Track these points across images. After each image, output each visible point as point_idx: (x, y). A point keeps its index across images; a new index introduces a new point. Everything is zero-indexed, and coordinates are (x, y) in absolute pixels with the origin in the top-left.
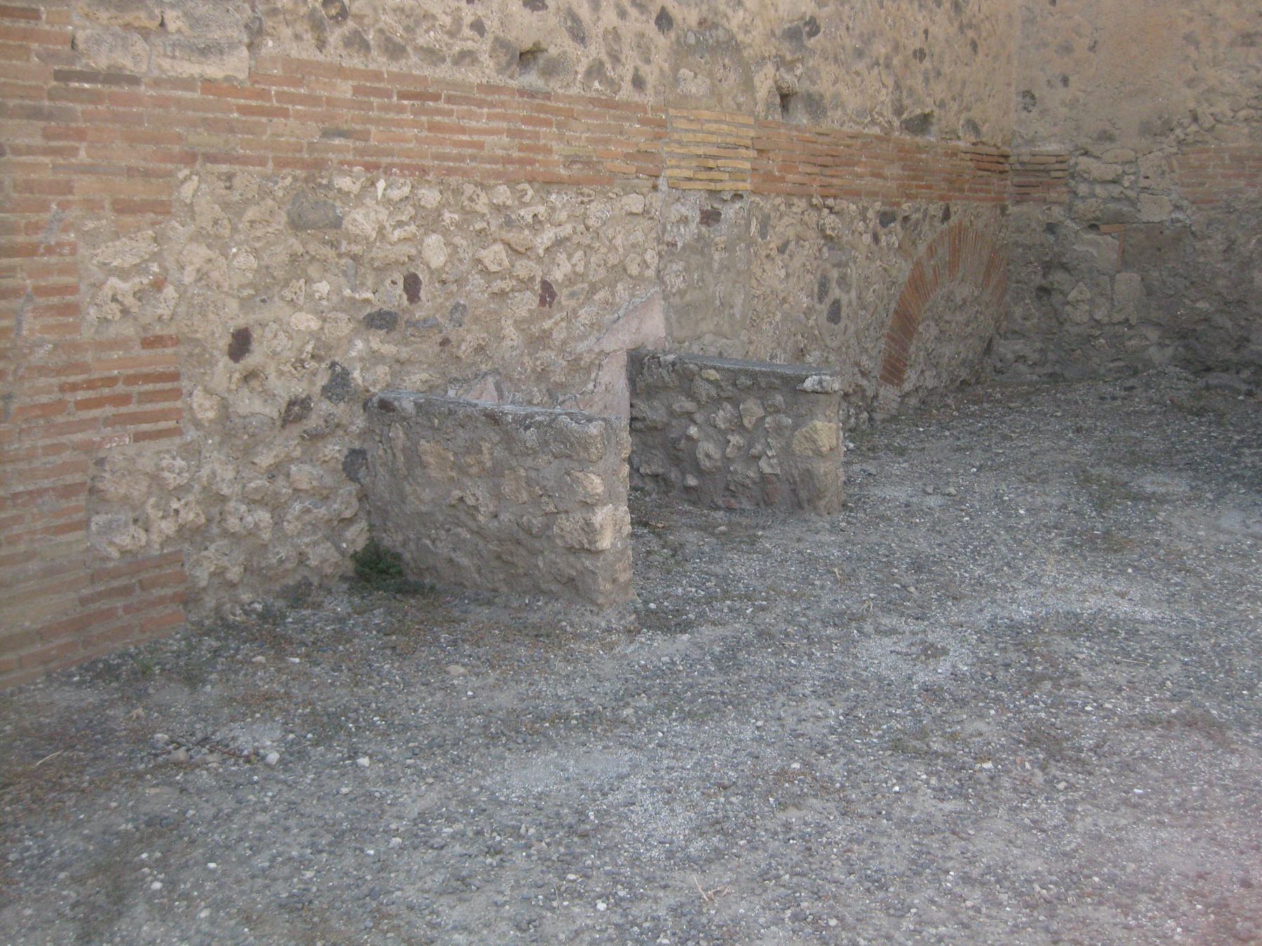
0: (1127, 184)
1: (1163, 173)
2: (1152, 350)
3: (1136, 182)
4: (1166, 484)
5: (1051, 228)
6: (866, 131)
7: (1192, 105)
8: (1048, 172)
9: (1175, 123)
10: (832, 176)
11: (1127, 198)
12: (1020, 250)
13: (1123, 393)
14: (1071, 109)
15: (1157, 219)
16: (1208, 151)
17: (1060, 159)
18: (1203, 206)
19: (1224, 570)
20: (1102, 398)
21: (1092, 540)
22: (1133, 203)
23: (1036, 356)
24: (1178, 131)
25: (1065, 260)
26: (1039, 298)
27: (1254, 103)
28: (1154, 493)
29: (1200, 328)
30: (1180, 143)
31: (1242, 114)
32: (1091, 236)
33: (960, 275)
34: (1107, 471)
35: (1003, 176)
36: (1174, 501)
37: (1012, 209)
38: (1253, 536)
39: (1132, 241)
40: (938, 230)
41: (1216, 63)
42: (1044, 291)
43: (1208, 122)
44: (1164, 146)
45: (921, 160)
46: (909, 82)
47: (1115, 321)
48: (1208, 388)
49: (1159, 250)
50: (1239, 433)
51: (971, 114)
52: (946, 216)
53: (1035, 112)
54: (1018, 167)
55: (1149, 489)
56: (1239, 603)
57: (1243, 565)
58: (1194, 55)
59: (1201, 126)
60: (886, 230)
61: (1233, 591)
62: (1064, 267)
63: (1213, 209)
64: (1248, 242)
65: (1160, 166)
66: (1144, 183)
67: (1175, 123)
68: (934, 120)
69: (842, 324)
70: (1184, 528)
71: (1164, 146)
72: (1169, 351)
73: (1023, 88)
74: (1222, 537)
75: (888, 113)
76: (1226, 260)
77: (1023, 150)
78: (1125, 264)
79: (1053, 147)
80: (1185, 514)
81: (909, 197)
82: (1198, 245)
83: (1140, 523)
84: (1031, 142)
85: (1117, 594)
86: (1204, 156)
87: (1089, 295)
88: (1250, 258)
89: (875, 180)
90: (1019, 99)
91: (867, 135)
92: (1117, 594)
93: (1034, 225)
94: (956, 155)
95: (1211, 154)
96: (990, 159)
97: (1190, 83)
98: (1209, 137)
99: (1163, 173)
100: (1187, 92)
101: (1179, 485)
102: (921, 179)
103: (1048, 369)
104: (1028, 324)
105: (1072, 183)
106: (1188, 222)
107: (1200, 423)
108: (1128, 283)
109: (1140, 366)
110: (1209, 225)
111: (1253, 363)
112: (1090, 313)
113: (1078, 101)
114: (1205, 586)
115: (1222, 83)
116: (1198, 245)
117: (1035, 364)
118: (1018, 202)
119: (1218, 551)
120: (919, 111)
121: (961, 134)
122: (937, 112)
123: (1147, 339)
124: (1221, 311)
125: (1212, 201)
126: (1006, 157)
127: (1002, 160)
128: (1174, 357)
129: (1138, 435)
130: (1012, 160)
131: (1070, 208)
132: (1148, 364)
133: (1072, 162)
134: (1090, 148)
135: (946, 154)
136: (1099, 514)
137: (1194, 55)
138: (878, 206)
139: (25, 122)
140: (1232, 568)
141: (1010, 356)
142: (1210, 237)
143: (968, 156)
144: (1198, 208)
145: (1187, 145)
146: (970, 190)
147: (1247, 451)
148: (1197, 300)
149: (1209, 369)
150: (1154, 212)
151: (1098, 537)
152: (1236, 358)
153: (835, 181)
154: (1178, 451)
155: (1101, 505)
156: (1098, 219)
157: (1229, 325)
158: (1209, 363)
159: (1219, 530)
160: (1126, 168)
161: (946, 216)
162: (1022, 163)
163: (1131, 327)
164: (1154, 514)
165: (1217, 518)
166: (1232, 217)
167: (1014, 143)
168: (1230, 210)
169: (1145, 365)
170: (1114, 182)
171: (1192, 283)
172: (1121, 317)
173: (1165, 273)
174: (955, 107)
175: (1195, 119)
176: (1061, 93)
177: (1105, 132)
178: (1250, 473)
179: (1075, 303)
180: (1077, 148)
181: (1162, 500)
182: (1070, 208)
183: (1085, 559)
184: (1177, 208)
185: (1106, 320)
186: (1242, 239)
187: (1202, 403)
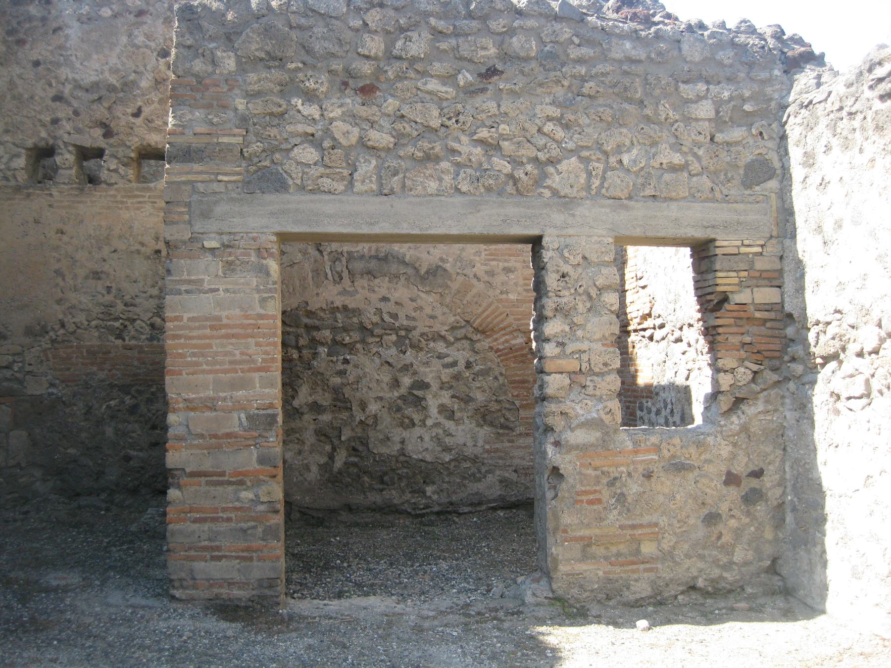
0: (16, 369)
1: (42, 361)
2: (38, 483)
3: (23, 367)
4: (65, 578)
7: (61, 317)
9: (49, 328)
11: (17, 379)
13: (21, 516)
15: (38, 393)
16: (72, 347)
18: (69, 384)
19: (119, 632)
20: (7, 521)
21: (23, 625)
22: (21, 382)
24: (52, 334)
27: (101, 316)
28: (58, 585)
30: (53, 341)
31: (94, 323)
34: (21, 575)
36: (74, 589)
38: (131, 606)
41: (76, 289)
43: (72, 328)
48: (79, 507)
49: (40, 414)
50: (106, 537)
55: (54, 583)
56: (134, 653)
57: (129, 627)
58: (62, 283)
61: (128, 645)
63: (77, 385)
64: (101, 406)
66: (28, 368)
67: (49, 328)
70: (85, 607)
74: (112, 610)
76: (86, 420)
80: (84, 597)
83: (55, 608)
85: (51, 660)
86: (69, 351)
92: (51, 660)
97: (59, 302)
98: (72, 338)
100: (57, 307)
101: (74, 578)
107: (79, 533)
110: (74, 396)
114: (109, 645)
115: (80, 302)
116: (67, 410)
119: (111, 619)
125: (76, 381)
129: (38, 545)
136: (24, 605)
137: (62, 283)
139: (213, 488)
140: (124, 630)
142: (75, 405)
145: (58, 343)
147: (114, 549)
149: (78, 495)
150: (36, 388)
151: (26, 622)
154: (68, 554)
155: (24, 600)
157: (91, 464)
159: (109, 605)
160: (16, 358)
163: (21, 469)
164: (62, 600)
165: (106, 597)
170: (7, 367)
171: (64, 436)
175: (63, 326)
178: (119, 564)
181: (66, 590)
183: (21, 640)
184: (52, 385)
187: (78, 518)
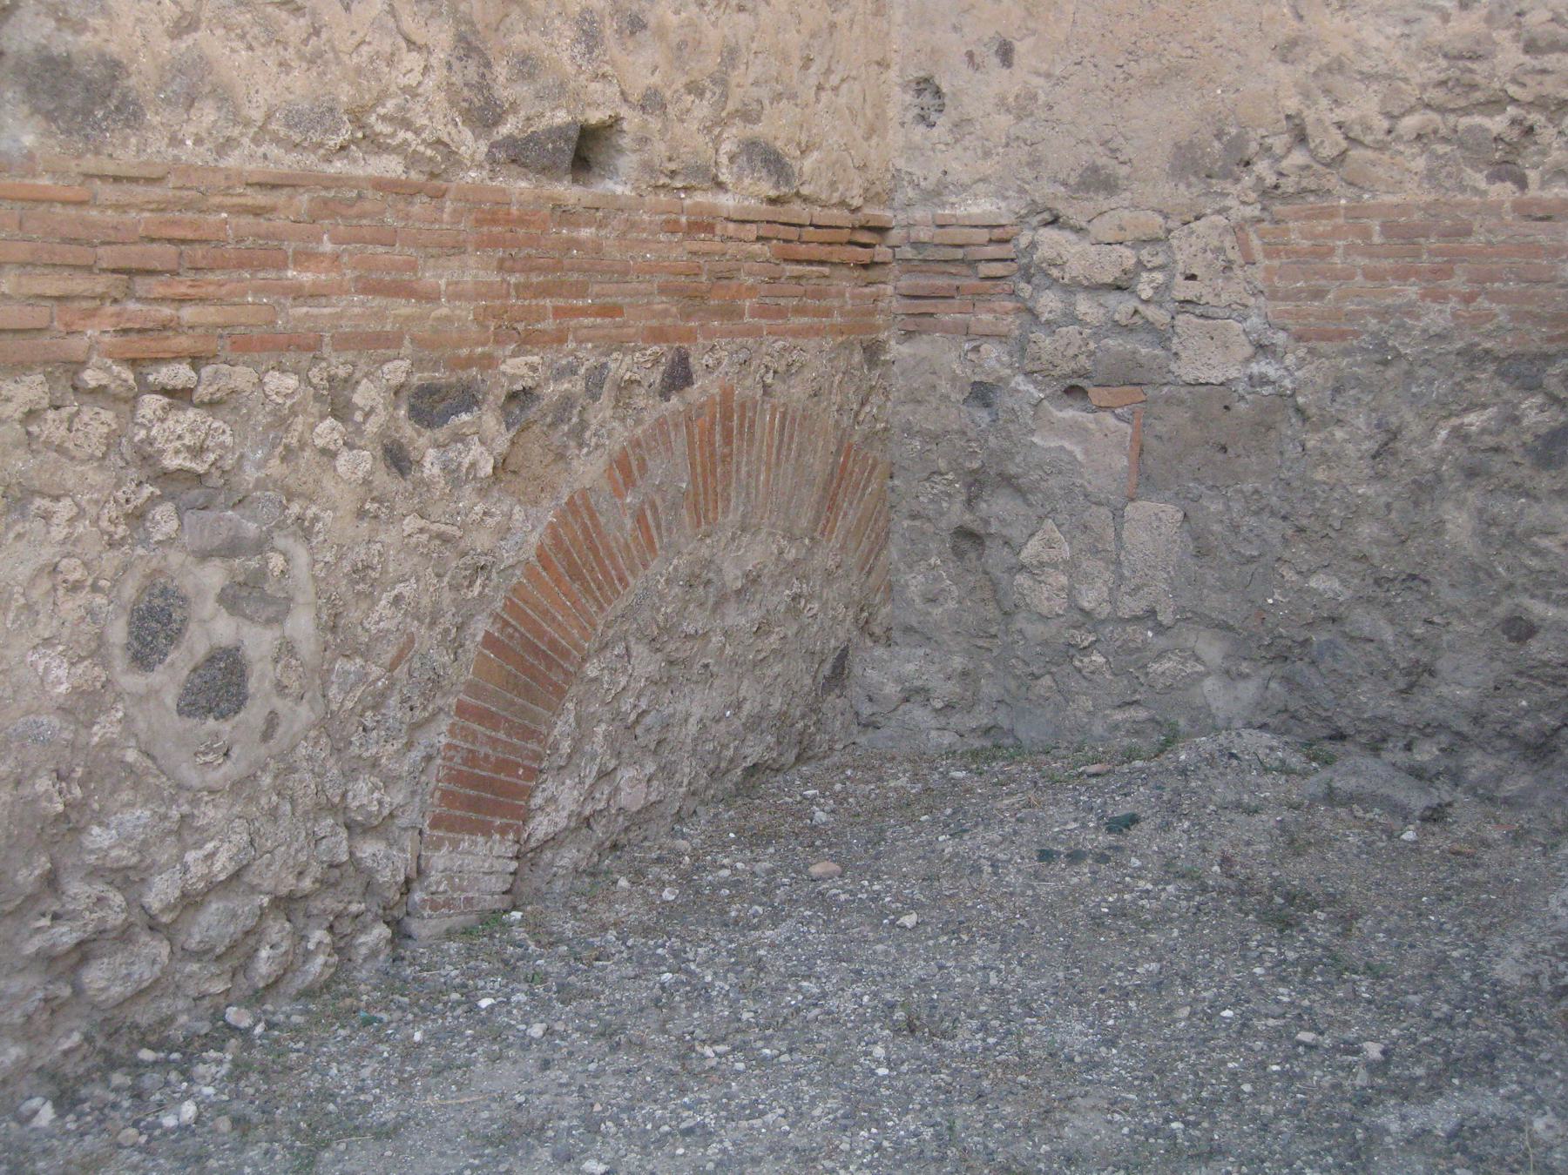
1: (1228, 267)
2: (1209, 684)
3: (1167, 286)
5: (982, 394)
6: (338, 166)
7: (1292, 104)
8: (972, 263)
9: (1253, 147)
10: (182, 300)
11: (1149, 326)
12: (917, 444)
14: (1019, 118)
15: (1216, 376)
16: (1330, 213)
17: (997, 233)
18: (1323, 346)
20: (1046, 856)
22: (1161, 336)
23: (952, 688)
24: (1262, 167)
25: (1012, 469)
26: (959, 554)
29: (1319, 637)
30: (1268, 193)
31: (1410, 123)
32: (1070, 413)
33: (734, 517)
35: (873, 274)
37: (897, 350)
39: (1160, 428)
40: (649, 418)
42: (969, 538)
43: (1331, 144)
44: (1229, 202)
45: (578, 244)
46: (519, 40)
47: (1125, 613)
49: (1224, 449)
51: (758, 130)
52: (679, 376)
53: (941, 131)
54: (908, 252)
59: (1313, 154)
60: (441, 434)
62: (1008, 481)
63: (1347, 353)
64: (1432, 431)
65: (1220, 250)
66: (1184, 290)
67: (1253, 147)
68: (626, 142)
69: (253, 714)
71: (1229, 202)
72: (1248, 690)
73: (914, 73)
75: (437, 120)
76: (1379, 477)
77: (919, 214)
78: (1144, 480)
79: (982, 207)
81: (527, 342)
82: (1312, 441)
84: (935, 195)
86: (1322, 226)
87: (1066, 551)
88: (1436, 472)
89: (376, 302)
90: (909, 98)
91: (338, 181)
93: (944, 387)
94: (710, 228)
95: (1340, 221)
96: (825, 235)
97: (1287, 51)
98: (1332, 181)
99: (1228, 267)
102: (580, 291)
103: (981, 718)
104: (937, 611)
105: (1026, 289)
106: (1287, 383)
108: (1153, 525)
109: (1182, 722)
110: (1337, 390)
111: (1442, 727)
112: (1071, 592)
113: (1034, 97)
115: (1361, 48)
117: (949, 706)
118: (909, 335)
120: (561, 117)
121: (725, 176)
122: (632, 121)
123: (1198, 659)
124: (1370, 600)
125: (1342, 335)
126: (881, 230)
127: (865, 237)
128: (1260, 705)
130: (895, 236)
131: (1022, 347)
132: (1205, 721)
133: (1024, 241)
134: (1061, 207)
135: (672, 227)
138: (396, 371)
141: (891, 689)
143: (751, 231)
144: (1311, 351)
145: (1286, 198)
146: (762, 311)
148: (1312, 572)
150: (1209, 359)
152: (1402, 713)
153: (188, 313)
156: (1086, 375)
157: (1388, 634)
158: (1342, 723)
160: (1145, 254)
161: (679, 376)
162: (916, 245)
163: (1160, 629)
166: (1390, 373)
167: (900, 197)
168: (1384, 355)
169: (1193, 721)
171: (1301, 530)
172: (1131, 605)
173: (1236, 506)
174: (703, 109)
176: (998, 81)
177: (1095, 170)
179: (1034, 570)
180: (1034, 209)
182: (1022, 347)
184: (1262, 349)
185: (1106, 609)
186: (1416, 428)
